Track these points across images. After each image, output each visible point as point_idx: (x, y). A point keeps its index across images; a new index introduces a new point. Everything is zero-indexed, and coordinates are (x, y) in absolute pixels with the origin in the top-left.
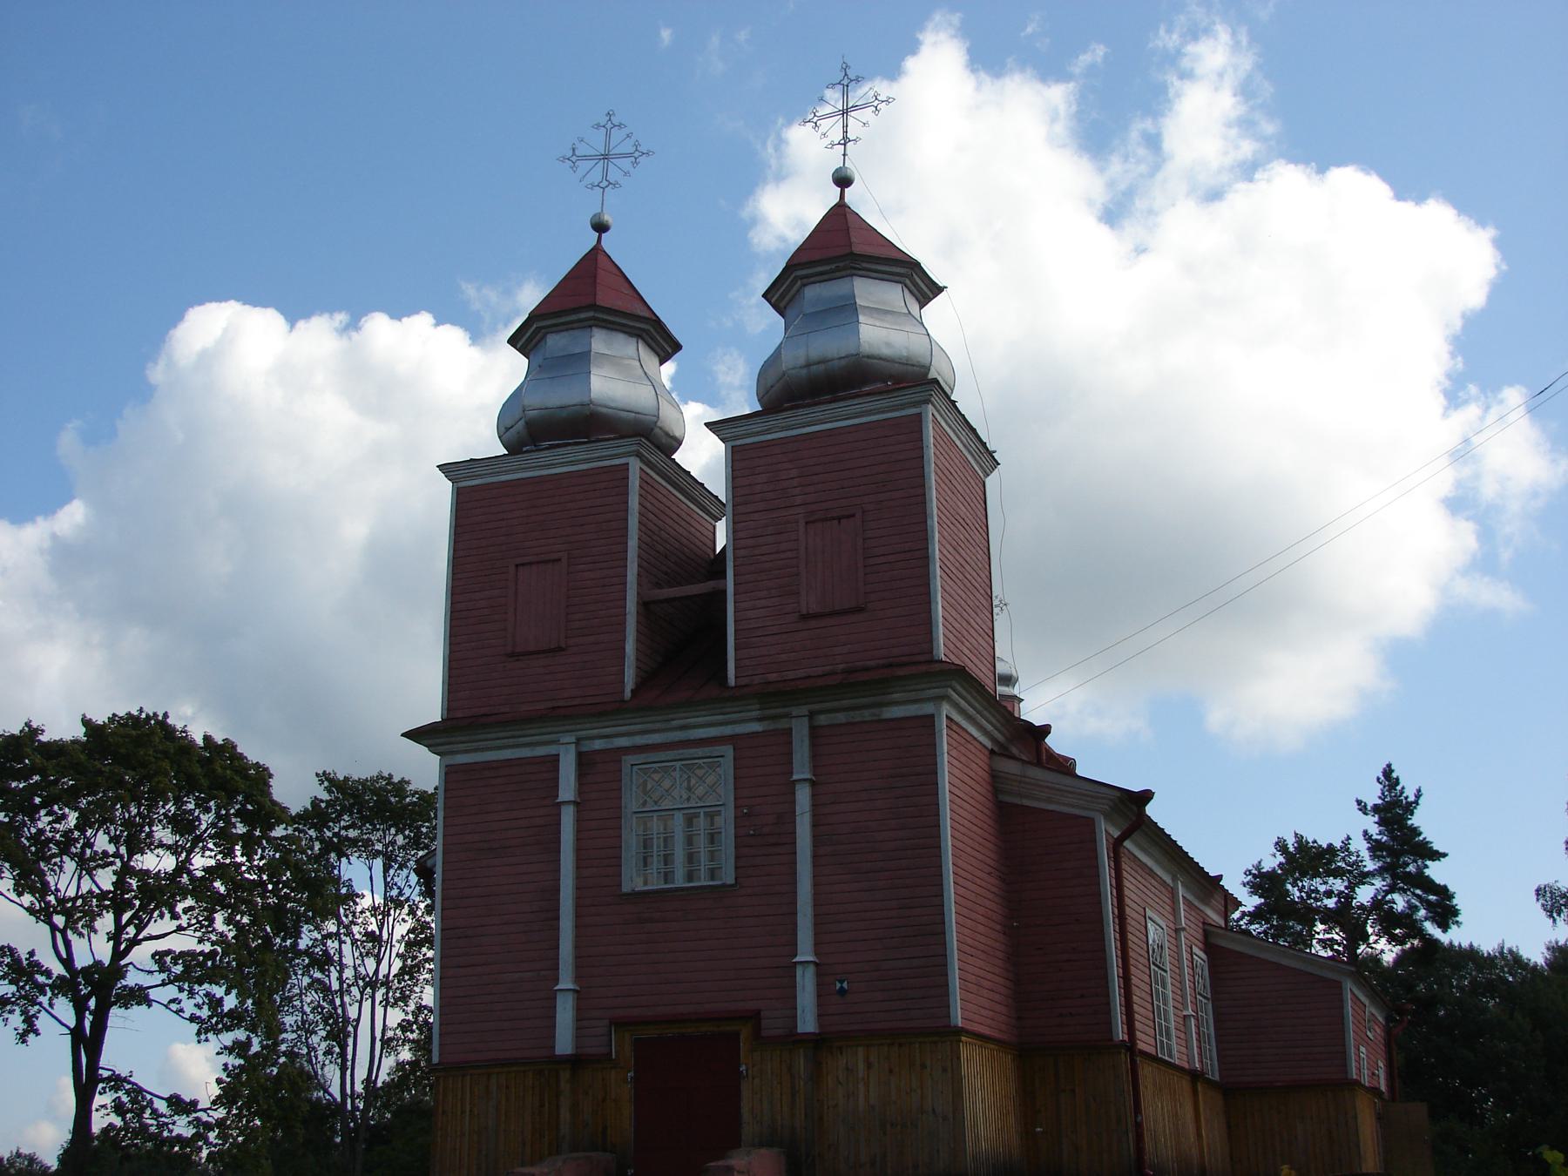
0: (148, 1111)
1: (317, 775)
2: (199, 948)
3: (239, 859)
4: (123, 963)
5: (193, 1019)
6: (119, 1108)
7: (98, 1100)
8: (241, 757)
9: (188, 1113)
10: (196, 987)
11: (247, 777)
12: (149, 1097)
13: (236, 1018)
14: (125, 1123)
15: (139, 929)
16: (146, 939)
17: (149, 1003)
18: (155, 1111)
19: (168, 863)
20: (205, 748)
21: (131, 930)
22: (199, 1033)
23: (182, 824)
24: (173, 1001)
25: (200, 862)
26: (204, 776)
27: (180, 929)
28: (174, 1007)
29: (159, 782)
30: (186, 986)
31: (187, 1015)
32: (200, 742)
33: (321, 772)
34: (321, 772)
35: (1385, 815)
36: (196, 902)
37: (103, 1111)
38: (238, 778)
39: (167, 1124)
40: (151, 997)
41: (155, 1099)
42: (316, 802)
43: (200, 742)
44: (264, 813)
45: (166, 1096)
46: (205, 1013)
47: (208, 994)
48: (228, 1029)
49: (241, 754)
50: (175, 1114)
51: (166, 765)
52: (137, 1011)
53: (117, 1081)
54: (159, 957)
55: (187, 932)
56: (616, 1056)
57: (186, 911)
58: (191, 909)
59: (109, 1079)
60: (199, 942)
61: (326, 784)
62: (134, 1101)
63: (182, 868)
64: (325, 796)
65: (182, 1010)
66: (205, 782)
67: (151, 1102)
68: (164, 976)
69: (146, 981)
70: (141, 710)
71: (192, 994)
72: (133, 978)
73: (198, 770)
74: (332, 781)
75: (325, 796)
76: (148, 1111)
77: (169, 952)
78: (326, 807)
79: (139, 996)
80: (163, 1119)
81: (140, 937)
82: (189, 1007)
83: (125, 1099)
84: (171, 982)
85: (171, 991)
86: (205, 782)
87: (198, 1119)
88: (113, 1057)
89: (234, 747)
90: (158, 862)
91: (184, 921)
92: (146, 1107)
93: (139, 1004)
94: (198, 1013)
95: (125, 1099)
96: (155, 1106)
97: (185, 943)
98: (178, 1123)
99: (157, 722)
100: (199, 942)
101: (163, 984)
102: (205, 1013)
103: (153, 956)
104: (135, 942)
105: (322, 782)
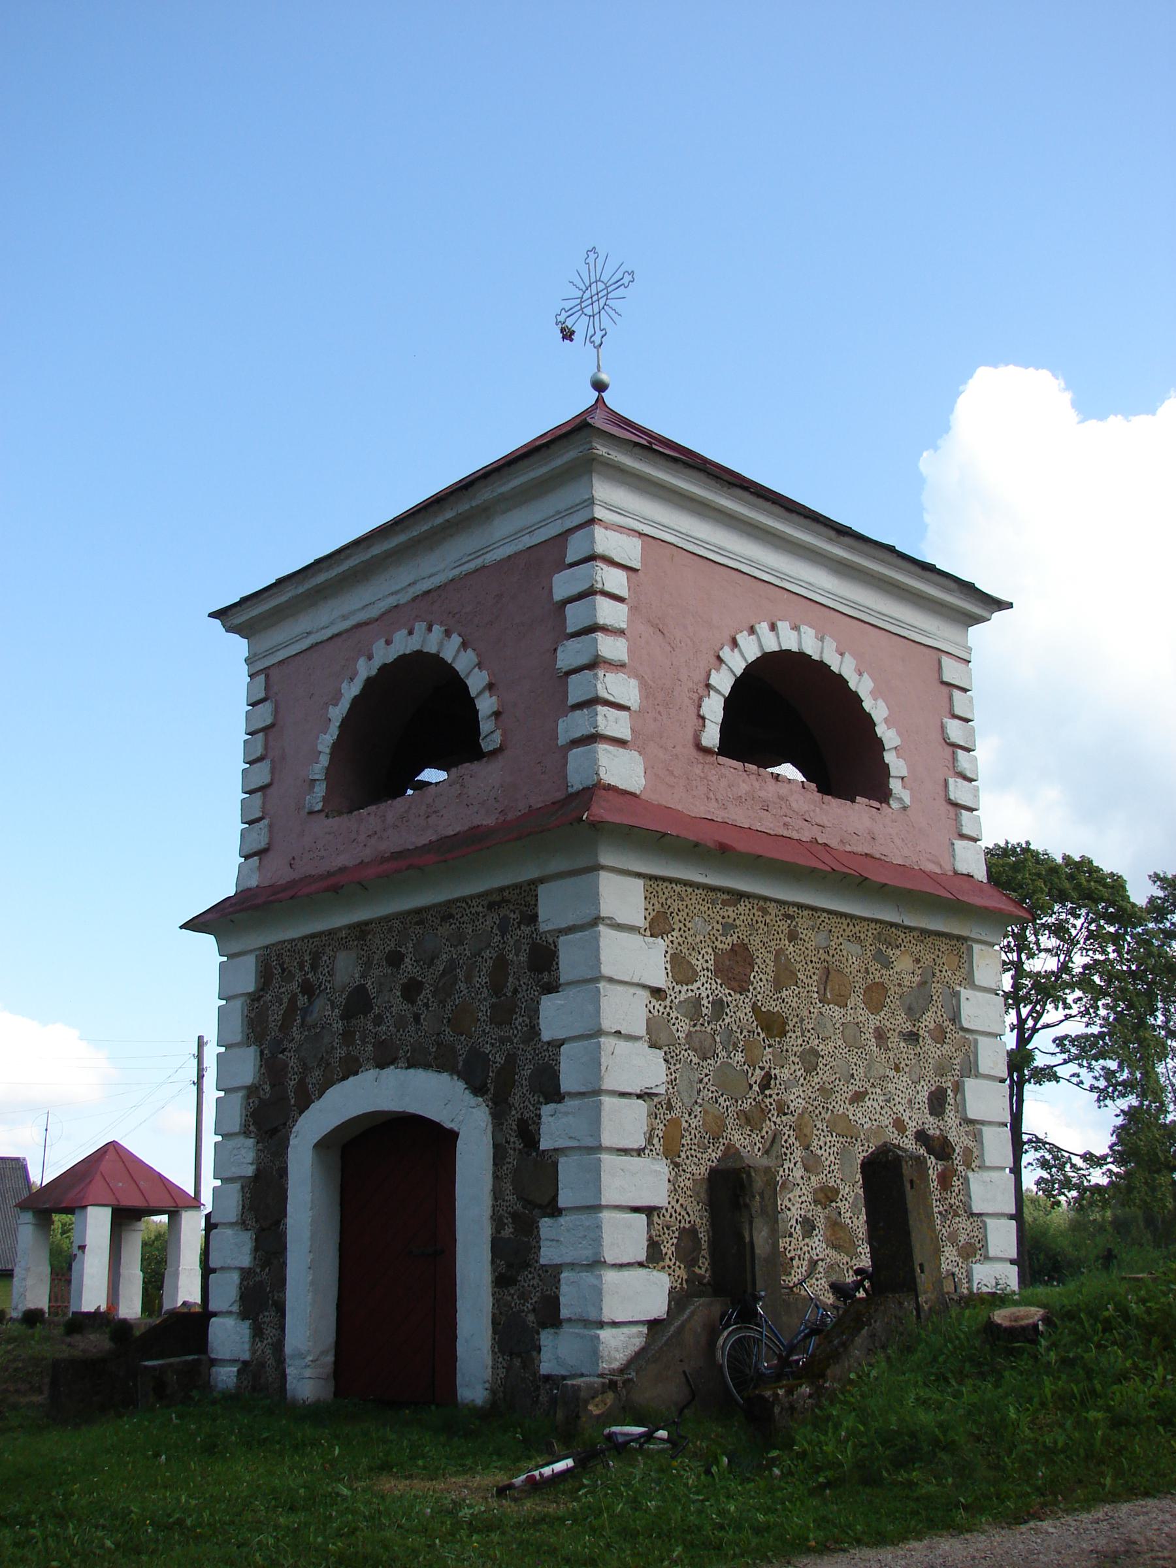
0: (1068, 1166)
1: (1150, 876)
2: (1089, 1031)
3: (1112, 956)
4: (1029, 1047)
5: (1092, 1088)
6: (1044, 1164)
7: (1026, 1159)
8: (1098, 870)
9: (1101, 1165)
10: (1093, 1062)
11: (1105, 885)
12: (1066, 1155)
13: (1128, 1087)
14: (1052, 1176)
15: (1036, 1020)
16: (1044, 1027)
17: (1057, 1079)
18: (1073, 1166)
19: (1052, 964)
20: (1067, 865)
21: (1030, 1023)
22: (1099, 1100)
23: (1059, 930)
24: (1073, 1075)
25: (1079, 961)
26: (1074, 889)
27: (1068, 1017)
28: (1075, 1080)
29: (1037, 899)
30: (1085, 1063)
31: (1086, 1086)
32: (1059, 860)
33: (1152, 874)
34: (1152, 874)
35: (1060, 1502)
36: (1084, 993)
37: (1030, 1167)
38: (1101, 888)
39: (1084, 1176)
40: (1058, 1074)
41: (1072, 1156)
42: (1152, 900)
43: (1059, 860)
44: (1125, 915)
45: (1081, 1153)
46: (1102, 1084)
47: (1103, 1068)
48: (1123, 1095)
49: (1097, 867)
50: (1091, 1167)
51: (1040, 883)
52: (1049, 1086)
53: (1038, 1143)
54: (1059, 1041)
55: (1076, 1019)
56: (146, 1367)
57: (1075, 1001)
58: (1080, 999)
59: (1030, 1141)
60: (1087, 1026)
61: (1158, 883)
62: (1055, 1158)
63: (1064, 968)
64: (1161, 894)
65: (1082, 1082)
66: (1074, 895)
67: (1070, 1158)
68: (1065, 1056)
69: (1052, 1061)
70: (1007, 843)
71: (1090, 1068)
72: (1040, 1061)
73: (1067, 885)
74: (1161, 880)
75: (1161, 894)
76: (1068, 1166)
77: (1066, 1037)
78: (1163, 903)
79: (1048, 1074)
80: (1082, 1172)
81: (1038, 1026)
82: (1087, 1078)
83: (1048, 1157)
84: (1070, 1061)
85: (1072, 1068)
86: (1074, 895)
87: (1109, 1170)
88: (1031, 1124)
89: (1090, 862)
90: (1043, 964)
91: (1074, 1011)
92: (1066, 1163)
93: (1049, 1080)
94: (1096, 1084)
95: (1048, 1157)
96: (1074, 1162)
97: (1076, 1028)
98: (1093, 1174)
99: (1022, 850)
100: (1087, 1026)
101: (1065, 1062)
102: (1102, 1084)
103: (1054, 1041)
104: (1035, 1030)
105: (1155, 882)
